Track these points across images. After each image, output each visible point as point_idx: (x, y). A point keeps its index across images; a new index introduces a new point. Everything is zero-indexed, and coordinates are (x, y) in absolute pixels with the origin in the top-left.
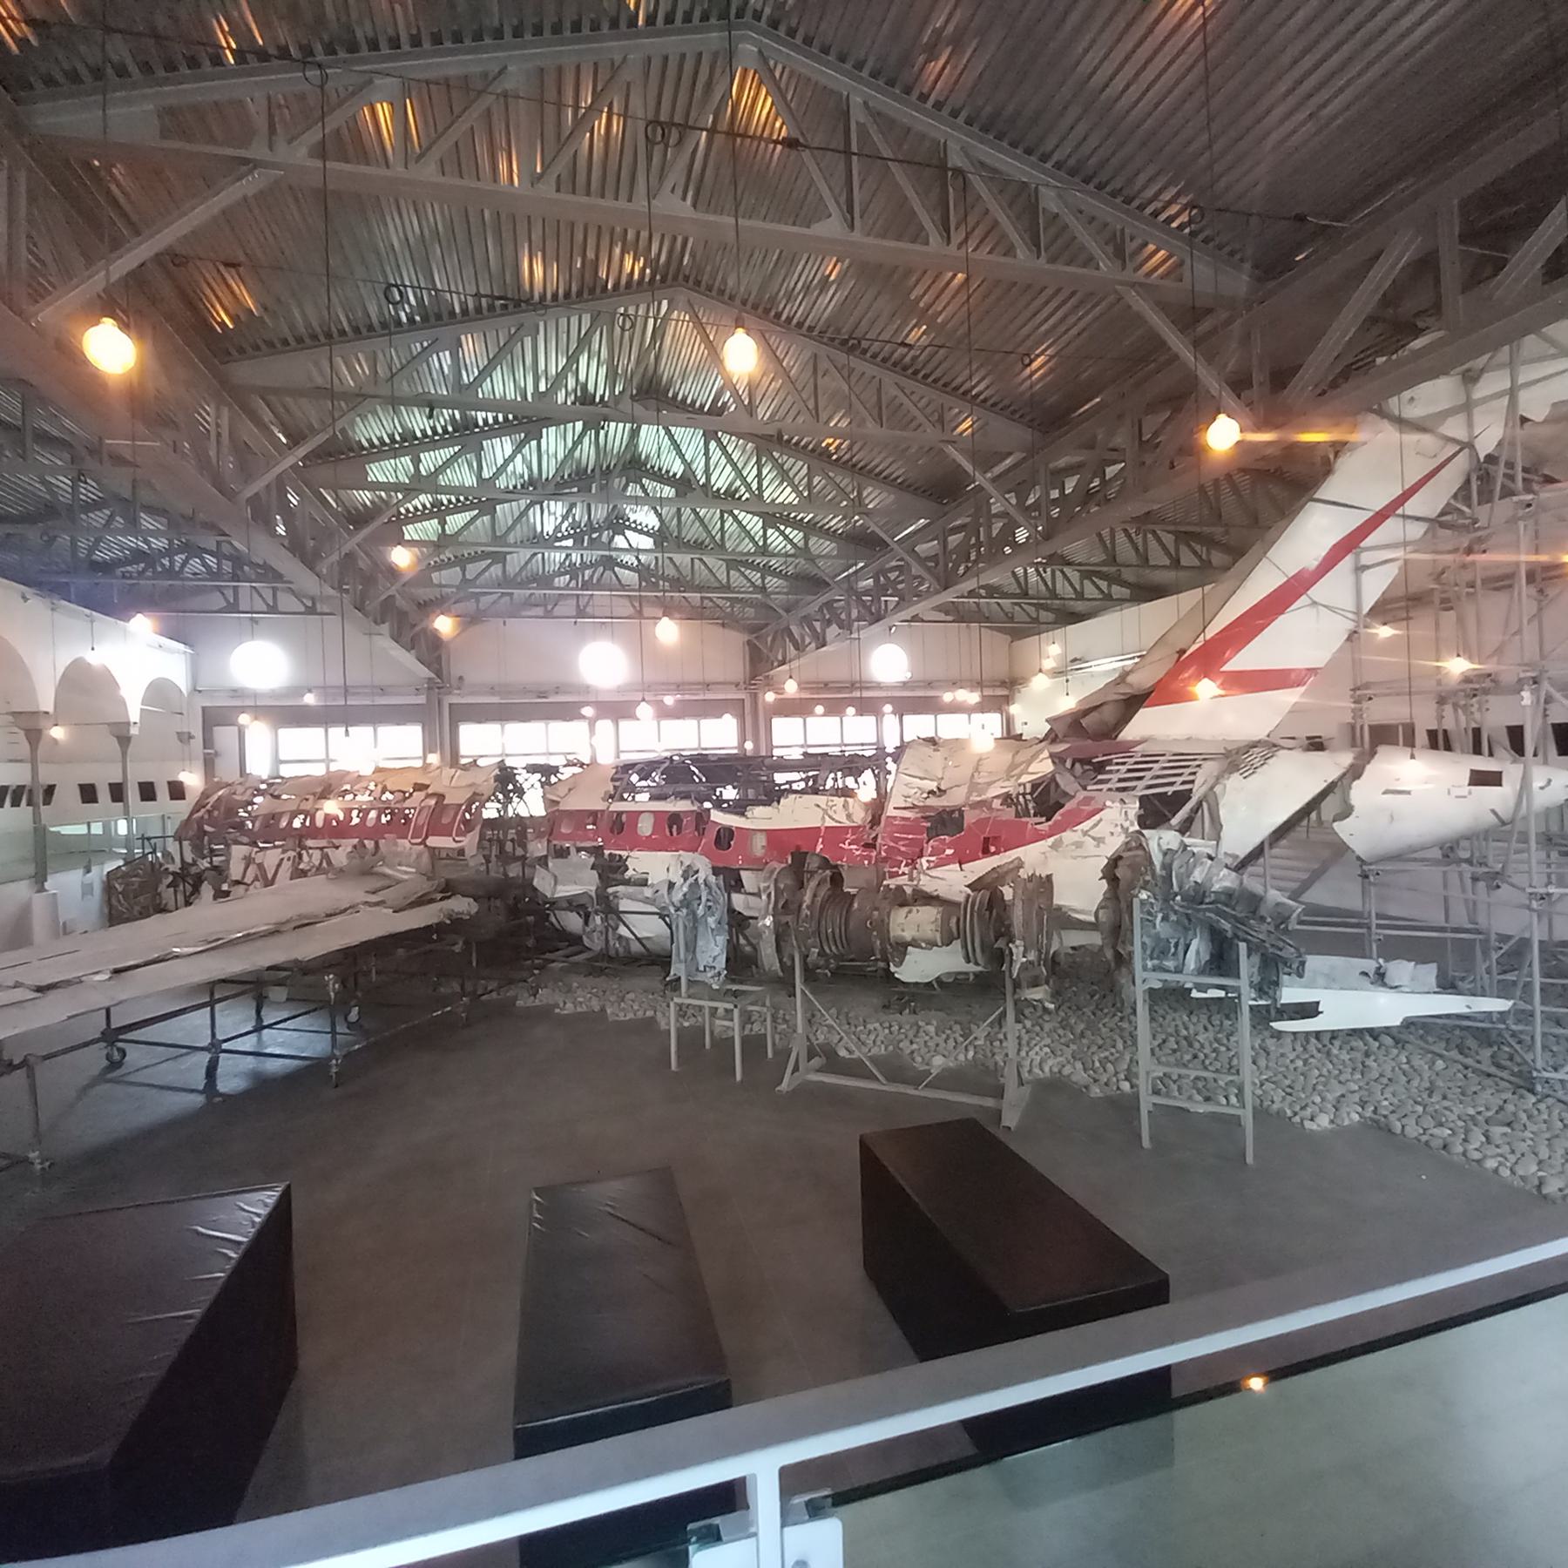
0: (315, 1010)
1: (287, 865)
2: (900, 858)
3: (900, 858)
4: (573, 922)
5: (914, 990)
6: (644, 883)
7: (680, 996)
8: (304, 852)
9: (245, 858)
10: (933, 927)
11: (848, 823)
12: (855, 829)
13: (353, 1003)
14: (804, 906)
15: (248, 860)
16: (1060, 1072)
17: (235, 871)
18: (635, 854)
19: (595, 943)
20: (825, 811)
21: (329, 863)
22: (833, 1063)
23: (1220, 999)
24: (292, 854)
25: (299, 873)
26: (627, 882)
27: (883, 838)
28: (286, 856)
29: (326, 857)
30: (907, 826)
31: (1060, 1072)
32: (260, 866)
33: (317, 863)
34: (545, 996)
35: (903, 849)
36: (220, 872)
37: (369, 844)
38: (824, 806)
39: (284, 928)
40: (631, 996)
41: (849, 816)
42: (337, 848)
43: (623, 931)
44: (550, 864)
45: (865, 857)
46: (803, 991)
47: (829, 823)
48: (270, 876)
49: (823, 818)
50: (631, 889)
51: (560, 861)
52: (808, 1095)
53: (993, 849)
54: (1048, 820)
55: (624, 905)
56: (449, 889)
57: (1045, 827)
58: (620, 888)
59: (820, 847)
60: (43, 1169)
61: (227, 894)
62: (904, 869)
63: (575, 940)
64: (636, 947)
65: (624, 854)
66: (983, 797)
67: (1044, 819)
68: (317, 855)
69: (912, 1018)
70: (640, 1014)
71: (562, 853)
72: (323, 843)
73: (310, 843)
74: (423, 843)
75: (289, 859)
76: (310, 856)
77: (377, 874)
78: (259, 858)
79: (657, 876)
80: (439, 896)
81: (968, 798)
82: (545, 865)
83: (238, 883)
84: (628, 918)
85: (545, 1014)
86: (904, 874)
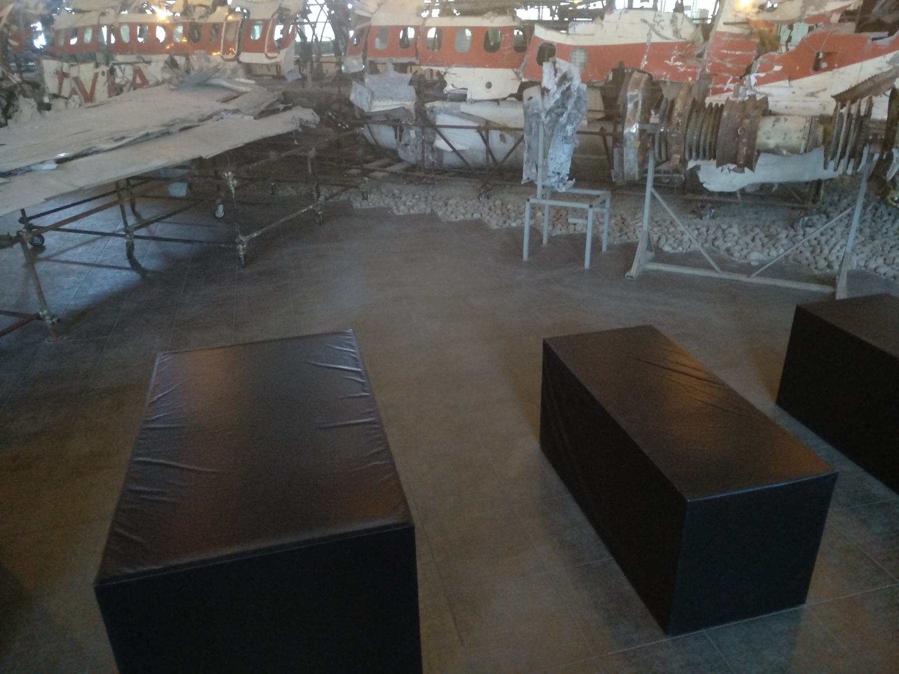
0: (186, 208)
1: (102, 79)
2: (726, 75)
3: (726, 75)
4: (386, 136)
5: (716, 198)
6: (462, 98)
7: (535, 197)
8: (116, 67)
9: (57, 72)
10: (801, 135)
11: (673, 39)
12: (682, 46)
13: (218, 201)
14: (675, 113)
15: (62, 76)
16: (866, 267)
17: (51, 84)
18: (454, 70)
19: (410, 155)
20: (652, 27)
21: (143, 77)
22: (660, 256)
23: (522, 256)
24: (104, 68)
25: (116, 90)
26: (444, 98)
27: (709, 54)
28: (100, 70)
29: (138, 72)
30: (736, 42)
31: (866, 267)
32: (77, 80)
33: (130, 78)
34: (374, 200)
35: (729, 66)
36: (36, 87)
37: (180, 60)
38: (650, 21)
39: (172, 130)
40: (452, 201)
41: (676, 32)
42: (149, 63)
43: (440, 143)
44: (367, 80)
45: (690, 74)
46: (653, 197)
47: (656, 39)
48: (88, 89)
49: (649, 35)
50: (447, 105)
51: (375, 77)
52: (648, 280)
53: (824, 65)
54: (891, 34)
55: (442, 119)
56: (287, 102)
57: (886, 42)
58: (438, 104)
59: (644, 63)
60: (53, 323)
61: (48, 107)
62: (730, 85)
63: (390, 155)
64: (450, 159)
65: (442, 69)
66: (822, 11)
67: (886, 34)
68: (129, 71)
69: (713, 223)
70: (469, 216)
71: (373, 69)
72: (132, 58)
73: (119, 58)
74: (236, 59)
75: (103, 73)
76: (123, 71)
77: (212, 86)
78: (73, 72)
79: (476, 91)
80: (281, 106)
81: (803, 13)
82: (362, 80)
83: (55, 96)
84: (446, 132)
85: (382, 215)
86: (729, 90)
